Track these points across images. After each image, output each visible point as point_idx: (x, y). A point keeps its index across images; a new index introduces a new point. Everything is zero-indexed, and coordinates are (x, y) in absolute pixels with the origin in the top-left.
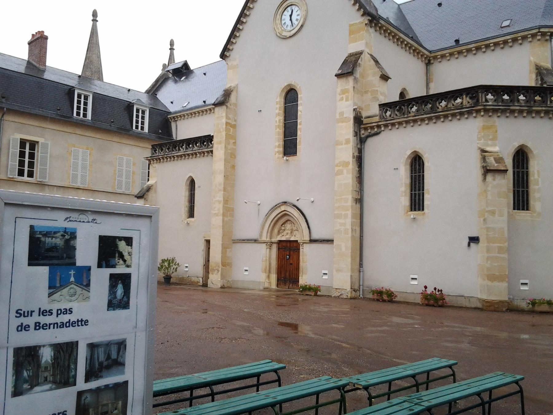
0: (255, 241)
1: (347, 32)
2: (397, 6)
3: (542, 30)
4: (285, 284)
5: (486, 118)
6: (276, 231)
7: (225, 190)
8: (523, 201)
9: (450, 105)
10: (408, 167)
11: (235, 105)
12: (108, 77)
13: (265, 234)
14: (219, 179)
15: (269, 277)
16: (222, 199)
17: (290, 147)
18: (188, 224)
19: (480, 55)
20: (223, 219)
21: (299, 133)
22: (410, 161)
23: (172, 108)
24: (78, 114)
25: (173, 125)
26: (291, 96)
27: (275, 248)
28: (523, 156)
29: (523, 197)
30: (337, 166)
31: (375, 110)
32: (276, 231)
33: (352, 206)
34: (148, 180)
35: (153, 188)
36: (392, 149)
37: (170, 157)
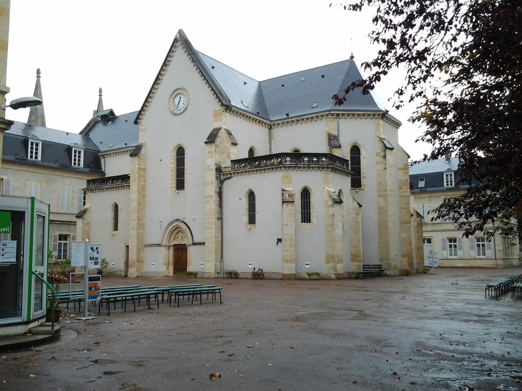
0: (159, 245)
1: (213, 115)
2: (257, 84)
3: (331, 112)
4: (178, 272)
5: (285, 171)
6: (172, 238)
7: (138, 212)
8: (307, 218)
9: (268, 163)
10: (247, 198)
11: (144, 155)
12: (49, 124)
13: (165, 240)
14: (135, 205)
15: (168, 268)
16: (136, 218)
17: (180, 185)
18: (114, 235)
19: (299, 125)
20: (137, 232)
21: (185, 175)
22: (248, 194)
23: (102, 149)
24: (31, 157)
25: (102, 161)
26: (180, 152)
27: (172, 249)
28: (307, 192)
29: (307, 215)
30: (206, 197)
31: (229, 164)
32: (172, 238)
33: (215, 222)
34: (84, 205)
35: (88, 210)
36: (238, 187)
37: (100, 189)
